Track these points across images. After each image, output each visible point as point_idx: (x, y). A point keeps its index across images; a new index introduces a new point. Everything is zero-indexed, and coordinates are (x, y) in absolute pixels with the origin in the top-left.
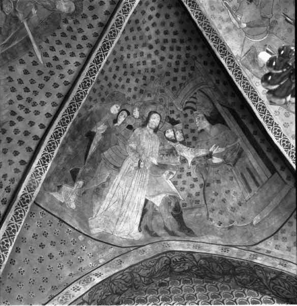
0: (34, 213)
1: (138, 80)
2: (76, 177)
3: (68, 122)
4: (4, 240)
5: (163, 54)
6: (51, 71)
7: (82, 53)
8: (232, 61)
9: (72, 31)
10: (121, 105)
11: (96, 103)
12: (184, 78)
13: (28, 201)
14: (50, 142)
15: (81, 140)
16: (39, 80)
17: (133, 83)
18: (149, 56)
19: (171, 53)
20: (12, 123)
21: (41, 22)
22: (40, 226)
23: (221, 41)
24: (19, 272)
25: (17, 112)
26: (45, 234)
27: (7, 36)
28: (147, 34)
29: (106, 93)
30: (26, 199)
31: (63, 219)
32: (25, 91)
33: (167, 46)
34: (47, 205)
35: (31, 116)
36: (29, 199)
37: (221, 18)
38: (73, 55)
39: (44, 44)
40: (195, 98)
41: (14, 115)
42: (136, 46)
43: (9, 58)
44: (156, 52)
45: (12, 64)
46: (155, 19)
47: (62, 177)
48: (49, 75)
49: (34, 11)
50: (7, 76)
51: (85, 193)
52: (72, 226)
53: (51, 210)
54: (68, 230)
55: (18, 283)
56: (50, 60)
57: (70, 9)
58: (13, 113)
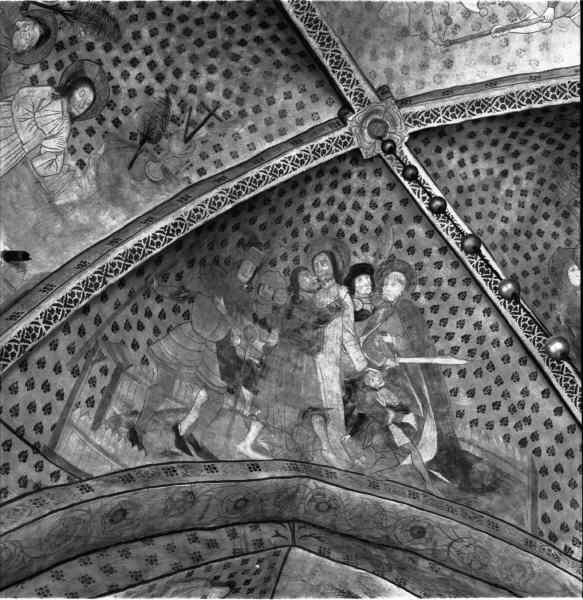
1: (546, 213)
5: (522, 158)
6: (482, 356)
7: (474, 298)
9: (434, 293)
10: (571, 261)
11: (555, 309)
16: (489, 379)
17: (546, 225)
18: (517, 181)
20: (537, 452)
23: (565, 85)
25: (523, 437)
27: (413, 398)
28: (483, 176)
29: (546, 282)
33: (515, 146)
37: (520, 52)
38: (470, 311)
39: (439, 346)
41: (526, 442)
42: (495, 201)
43: (445, 410)
44: (517, 167)
45: (454, 411)
46: (466, 156)
48: (487, 362)
49: (388, 339)
50: (468, 426)
57: (400, 281)
58: (523, 443)
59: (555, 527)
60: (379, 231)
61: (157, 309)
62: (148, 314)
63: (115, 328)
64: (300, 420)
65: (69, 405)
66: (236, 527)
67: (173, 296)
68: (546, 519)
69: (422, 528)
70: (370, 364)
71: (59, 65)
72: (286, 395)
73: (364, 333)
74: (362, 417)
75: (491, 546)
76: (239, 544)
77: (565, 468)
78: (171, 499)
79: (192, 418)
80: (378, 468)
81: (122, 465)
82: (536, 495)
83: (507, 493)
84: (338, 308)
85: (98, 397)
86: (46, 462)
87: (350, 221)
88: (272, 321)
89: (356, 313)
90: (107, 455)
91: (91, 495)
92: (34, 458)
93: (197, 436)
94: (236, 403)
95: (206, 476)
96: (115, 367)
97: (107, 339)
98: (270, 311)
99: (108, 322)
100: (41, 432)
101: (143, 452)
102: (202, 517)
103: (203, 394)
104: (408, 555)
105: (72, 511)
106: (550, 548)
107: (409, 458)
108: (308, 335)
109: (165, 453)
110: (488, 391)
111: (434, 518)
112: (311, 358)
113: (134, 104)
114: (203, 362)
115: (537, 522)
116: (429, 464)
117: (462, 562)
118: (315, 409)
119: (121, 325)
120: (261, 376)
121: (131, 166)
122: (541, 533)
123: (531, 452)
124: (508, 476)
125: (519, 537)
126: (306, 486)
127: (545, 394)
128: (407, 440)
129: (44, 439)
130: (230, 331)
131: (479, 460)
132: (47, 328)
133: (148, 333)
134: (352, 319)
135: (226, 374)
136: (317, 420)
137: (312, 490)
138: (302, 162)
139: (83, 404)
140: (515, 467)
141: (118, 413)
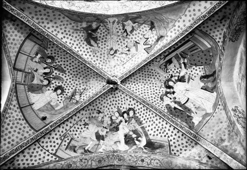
8: (148, 58)
12: (156, 73)
13: (195, 136)
19: (147, 77)
40: (163, 69)
58: (165, 136)
60: (125, 104)
62: (78, 128)
67: (83, 125)
71: (53, 87)
84: (121, 121)
87: (119, 104)
92: (51, 155)
96: (71, 138)
98: (107, 125)
113: (69, 91)
116: (144, 146)
121: (70, 101)
127: (166, 124)
128: (139, 143)
138: (101, 92)
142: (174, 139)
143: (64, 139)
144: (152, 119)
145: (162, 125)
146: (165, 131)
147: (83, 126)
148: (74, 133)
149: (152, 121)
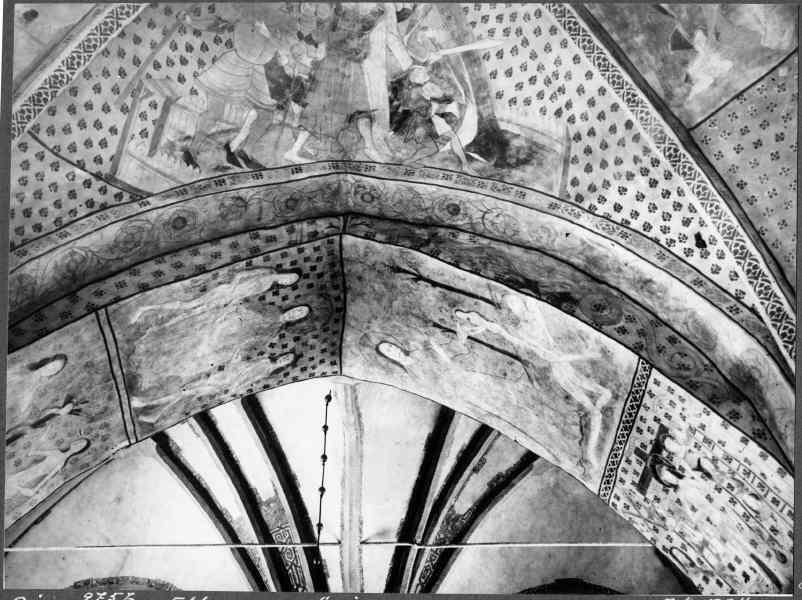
0: (706, 137)
2: (686, 42)
3: (590, 42)
4: (708, 209)
13: (676, 150)
14: (611, 80)
15: (632, 13)
16: (524, 55)
20: (571, 120)
21: (446, 26)
22: (729, 134)
24: (771, 197)
26: (745, 131)
27: (456, 88)
30: (672, 151)
31: (737, 92)
32: (534, 84)
34: (703, 112)
35: (571, 87)
36: (674, 146)
39: (477, 31)
41: (566, 106)
43: (485, 94)
45: (493, 94)
47: (674, 68)
49: (430, 34)
50: (507, 104)
51: (717, 35)
52: (755, 80)
53: (714, 107)
54: (759, 89)
55: (784, 206)
56: (500, 28)
59: (583, 189)
61: (197, 43)
63: (157, 66)
64: (347, 124)
65: (123, 140)
66: (295, 224)
67: (210, 29)
68: (575, 182)
69: (456, 205)
70: (415, 62)
72: (334, 103)
73: (407, 33)
74: (407, 114)
75: (516, 213)
76: (295, 237)
77: (597, 131)
78: (222, 204)
79: (241, 137)
80: (417, 157)
81: (179, 182)
82: (567, 161)
83: (540, 164)
85: (151, 129)
86: (109, 187)
88: (317, 36)
89: (398, 13)
90: (165, 175)
91: (148, 207)
92: (97, 184)
93: (248, 151)
94: (285, 117)
95: (252, 182)
96: (163, 100)
97: (150, 77)
99: (148, 61)
100: (101, 163)
101: (197, 170)
102: (259, 219)
103: (253, 113)
104: (450, 231)
105: (131, 221)
106: (574, 208)
107: (448, 144)
108: (353, 44)
109: (217, 168)
110: (524, 68)
111: (464, 196)
112: (357, 65)
114: (252, 85)
115: (566, 186)
116: (468, 147)
117: (498, 231)
118: (360, 113)
119: (163, 63)
120: (310, 90)
122: (569, 196)
123: (565, 121)
124: (543, 147)
125: (545, 202)
126: (346, 181)
128: (448, 128)
129: (105, 168)
130: (276, 53)
131: (517, 136)
132: (73, 74)
133: (193, 66)
134: (395, 20)
135: (276, 92)
136: (362, 123)
137: (352, 185)
139: (137, 136)
140: (551, 138)
141: (172, 140)
142: (589, 134)
143: (133, 105)
144: (520, 22)
145: (558, 62)
146: (561, 90)
147: (208, 38)
148: (174, 72)
149: (519, 31)
